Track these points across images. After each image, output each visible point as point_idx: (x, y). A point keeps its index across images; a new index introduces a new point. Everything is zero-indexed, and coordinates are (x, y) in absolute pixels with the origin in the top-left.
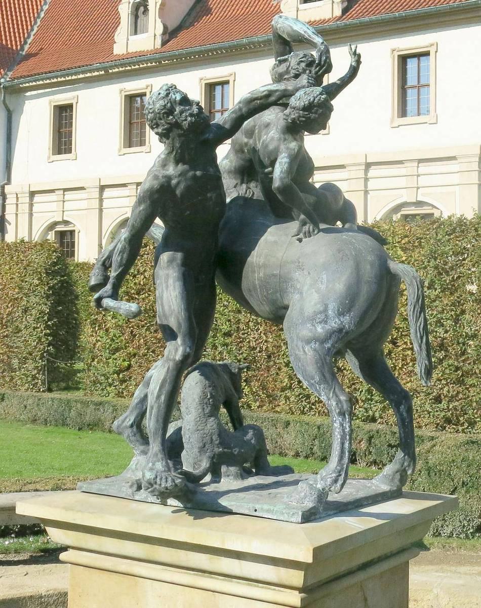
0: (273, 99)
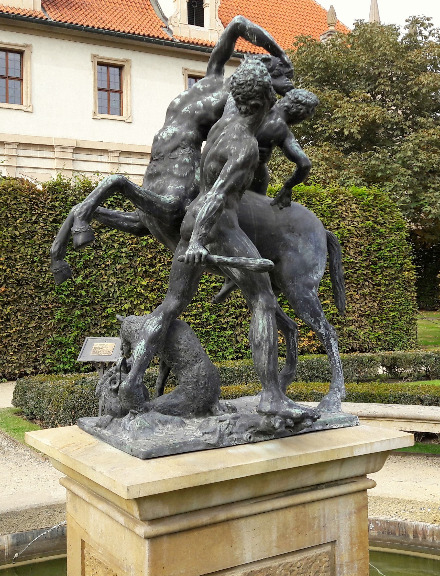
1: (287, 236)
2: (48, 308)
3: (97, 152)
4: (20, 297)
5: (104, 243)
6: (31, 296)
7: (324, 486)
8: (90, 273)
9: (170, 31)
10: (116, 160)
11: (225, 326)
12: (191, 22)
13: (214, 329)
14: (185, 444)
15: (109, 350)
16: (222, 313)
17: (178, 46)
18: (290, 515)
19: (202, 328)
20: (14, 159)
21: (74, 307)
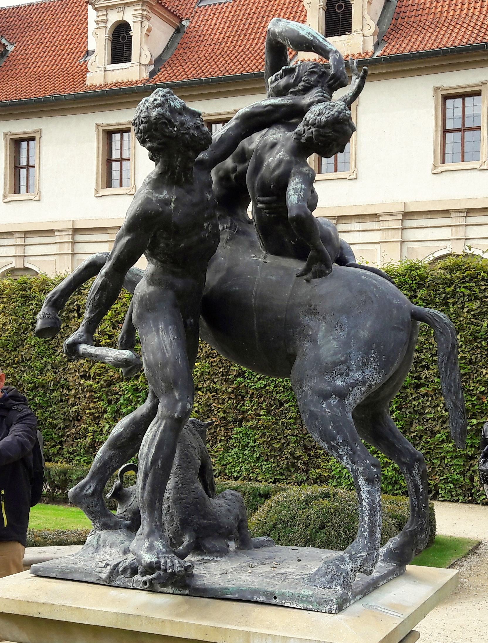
0: (277, 115)
1: (306, 320)
3: (351, 219)
14: (77, 570)
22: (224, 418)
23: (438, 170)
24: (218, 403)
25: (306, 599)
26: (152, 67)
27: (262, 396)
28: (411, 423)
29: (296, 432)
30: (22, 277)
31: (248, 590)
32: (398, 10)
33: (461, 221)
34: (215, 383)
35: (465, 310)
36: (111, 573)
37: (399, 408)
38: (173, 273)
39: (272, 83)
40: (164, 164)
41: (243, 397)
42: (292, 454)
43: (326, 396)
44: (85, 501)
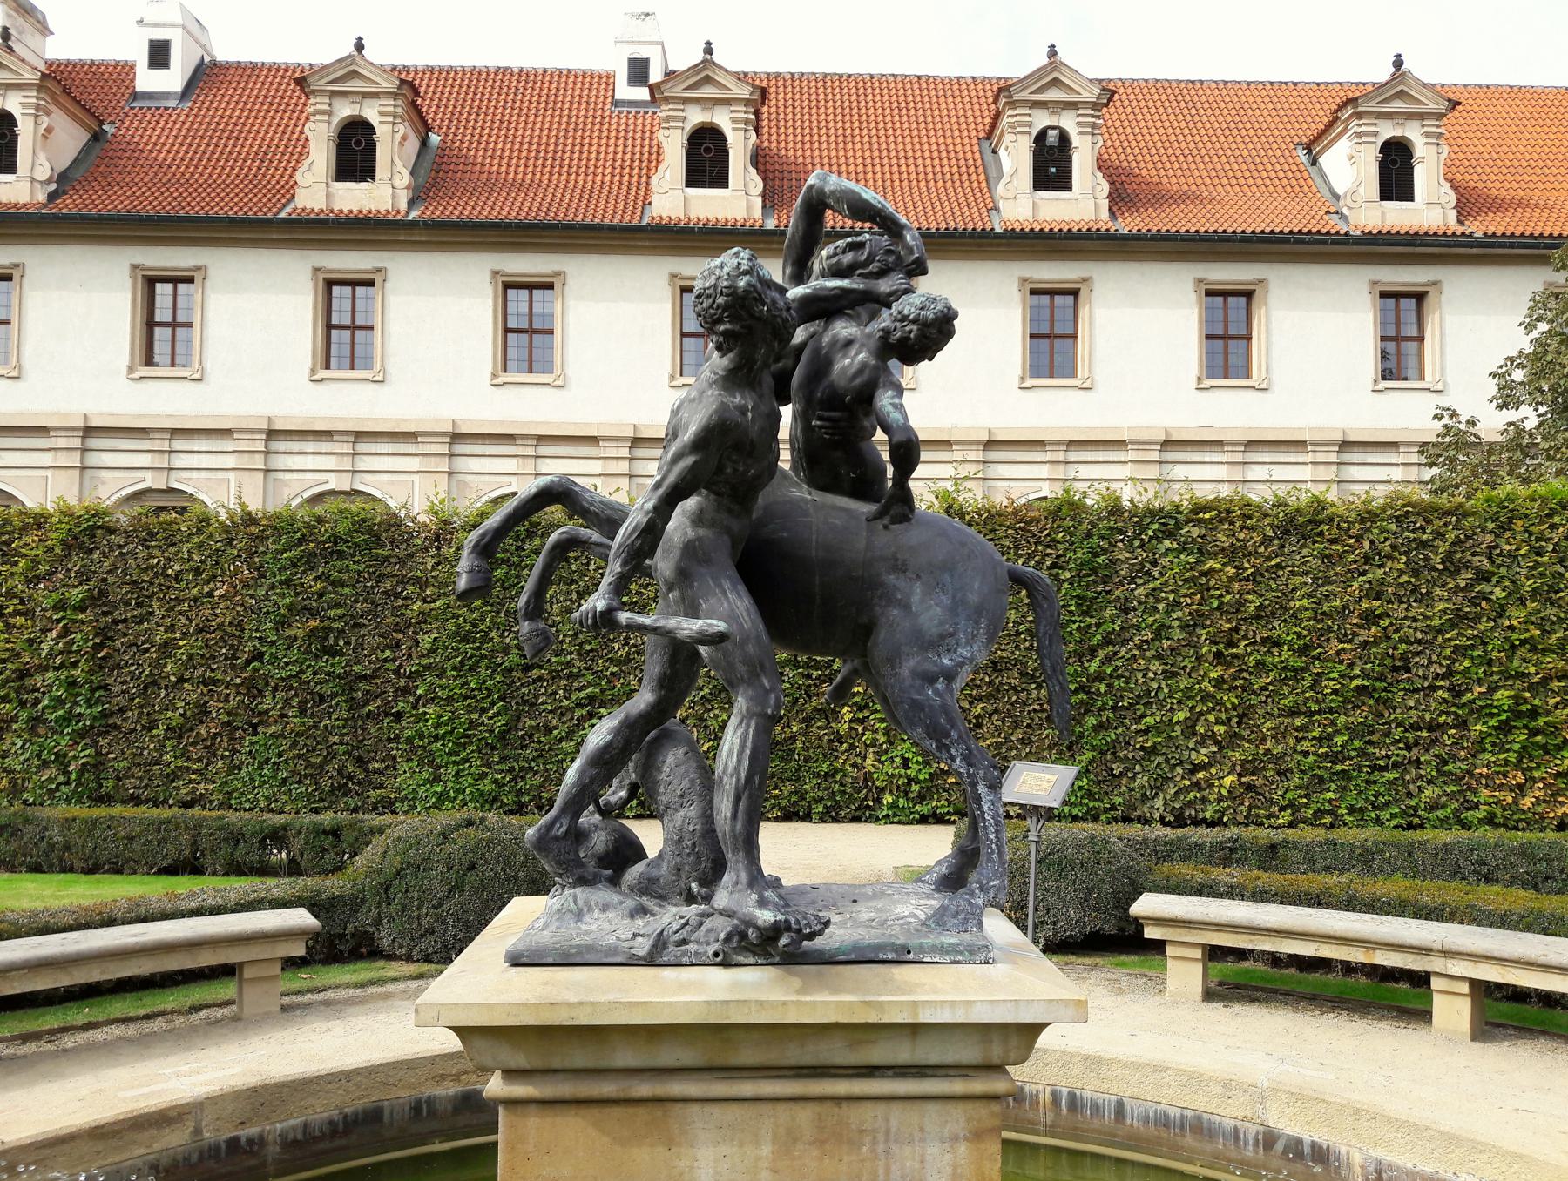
1: (891, 579)
2: (1043, 711)
4: (998, 690)
5: (1140, 603)
6: (1014, 688)
7: (890, 1073)
8: (1115, 654)
9: (1344, 218)
10: (1238, 458)
11: (1382, 763)
12: (1386, 195)
13: (1359, 768)
15: (1046, 785)
16: (1374, 738)
17: (1357, 242)
18: (805, 1114)
19: (1334, 763)
20: (1062, 467)
21: (1087, 711)
22: (229, 723)
23: (318, 377)
24: (218, 701)
25: (953, 949)
26: (53, 187)
27: (291, 688)
28: (518, 718)
29: (347, 738)
30: (356, 506)
31: (869, 946)
32: (438, 160)
33: (530, 451)
34: (213, 671)
35: (592, 567)
36: (654, 946)
37: (501, 699)
38: (730, 511)
39: (829, 257)
40: (741, 356)
41: (260, 692)
42: (340, 771)
43: (931, 679)
44: (554, 846)
